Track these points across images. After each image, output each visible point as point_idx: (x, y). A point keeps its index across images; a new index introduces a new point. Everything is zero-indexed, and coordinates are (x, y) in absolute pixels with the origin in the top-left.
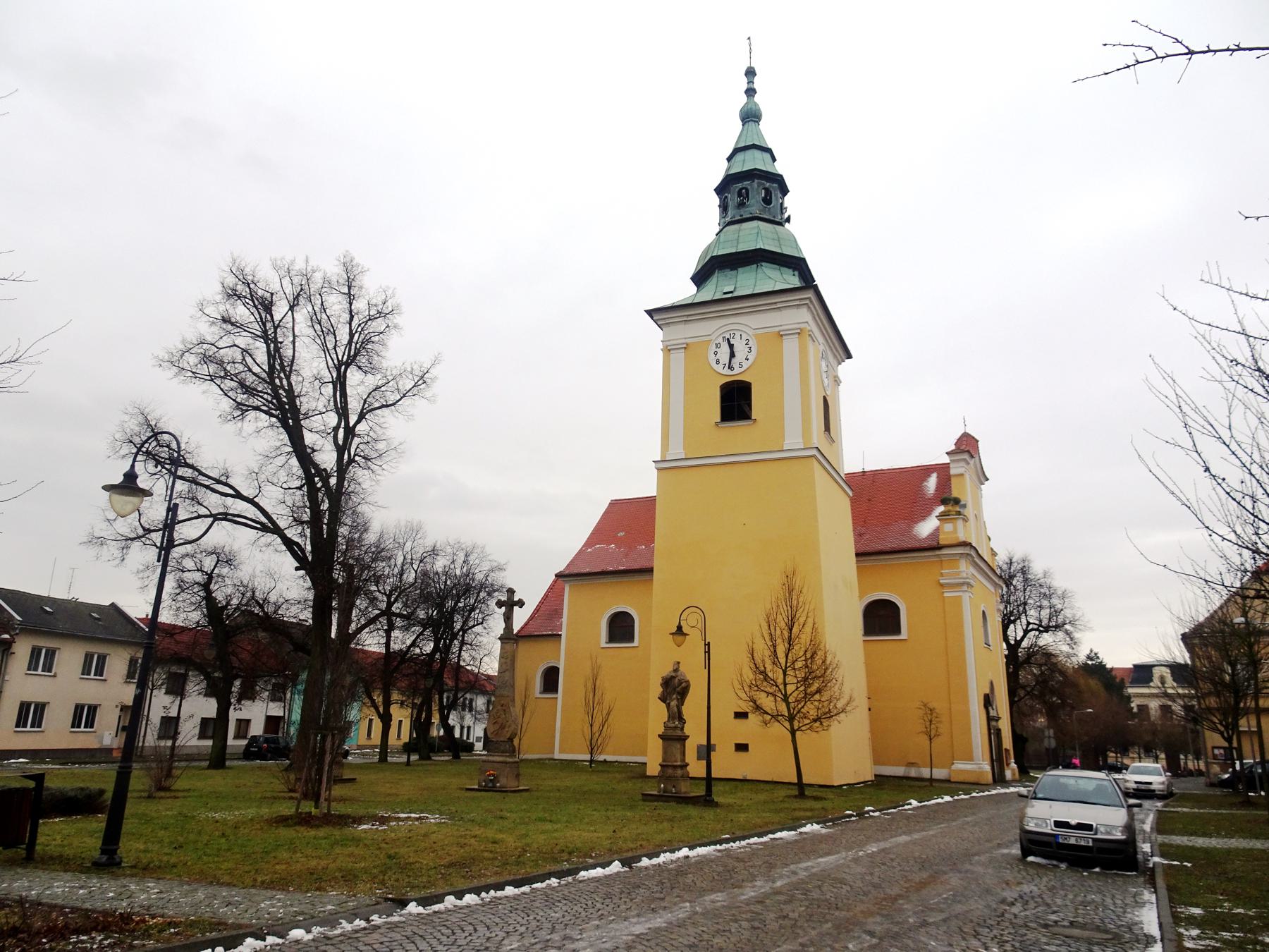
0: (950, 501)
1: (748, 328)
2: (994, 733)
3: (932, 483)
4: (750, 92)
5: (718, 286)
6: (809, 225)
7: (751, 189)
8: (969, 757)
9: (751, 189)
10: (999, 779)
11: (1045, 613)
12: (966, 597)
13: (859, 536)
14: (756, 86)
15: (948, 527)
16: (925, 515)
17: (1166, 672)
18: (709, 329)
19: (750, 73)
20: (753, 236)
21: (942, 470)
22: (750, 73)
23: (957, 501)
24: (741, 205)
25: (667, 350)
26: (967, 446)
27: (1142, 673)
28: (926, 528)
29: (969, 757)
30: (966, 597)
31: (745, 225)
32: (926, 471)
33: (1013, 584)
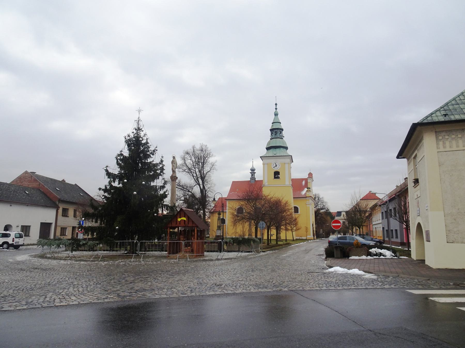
0: (306, 186)
1: (279, 161)
2: (313, 230)
3: (304, 182)
4: (276, 109)
5: (272, 153)
6: (288, 138)
7: (276, 132)
8: (310, 235)
9: (276, 132)
10: (314, 239)
11: (322, 206)
12: (311, 206)
13: (294, 195)
14: (277, 107)
15: (308, 193)
16: (303, 190)
17: (344, 213)
18: (272, 161)
19: (276, 104)
20: (277, 142)
21: (306, 180)
22: (276, 104)
23: (309, 188)
24: (276, 135)
25: (263, 164)
26: (310, 175)
27: (339, 213)
28: (304, 192)
29: (310, 235)
30: (311, 206)
31: (277, 139)
32: (302, 180)
33: (316, 199)
